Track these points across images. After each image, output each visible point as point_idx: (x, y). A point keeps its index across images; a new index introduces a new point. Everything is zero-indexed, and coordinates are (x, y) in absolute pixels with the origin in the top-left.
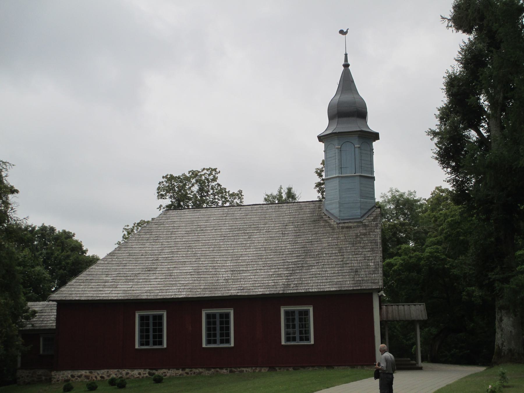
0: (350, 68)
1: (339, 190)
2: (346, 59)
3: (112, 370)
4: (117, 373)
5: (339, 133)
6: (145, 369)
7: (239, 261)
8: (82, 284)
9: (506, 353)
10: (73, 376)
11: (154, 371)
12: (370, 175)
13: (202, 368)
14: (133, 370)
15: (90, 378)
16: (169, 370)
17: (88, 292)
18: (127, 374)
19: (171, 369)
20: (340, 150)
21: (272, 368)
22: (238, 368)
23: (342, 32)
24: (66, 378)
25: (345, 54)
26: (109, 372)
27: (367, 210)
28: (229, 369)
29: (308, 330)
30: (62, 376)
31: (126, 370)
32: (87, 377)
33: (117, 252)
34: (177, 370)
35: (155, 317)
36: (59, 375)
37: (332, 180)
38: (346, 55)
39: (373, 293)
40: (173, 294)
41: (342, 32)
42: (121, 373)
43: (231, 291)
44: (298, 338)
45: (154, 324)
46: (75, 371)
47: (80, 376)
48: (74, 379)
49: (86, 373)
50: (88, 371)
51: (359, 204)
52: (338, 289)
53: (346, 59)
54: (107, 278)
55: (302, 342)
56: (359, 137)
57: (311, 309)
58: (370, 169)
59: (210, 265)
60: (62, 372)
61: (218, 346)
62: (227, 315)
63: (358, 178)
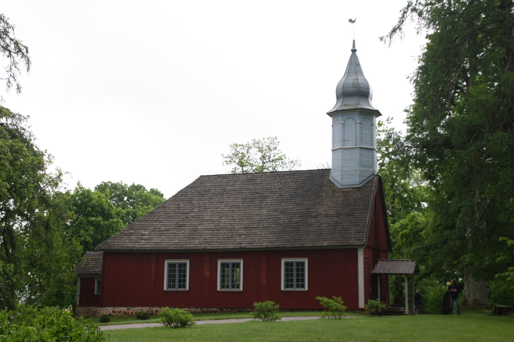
1: (342, 160)
2: (354, 46)
3: (144, 308)
5: (342, 110)
7: (252, 220)
8: (124, 237)
9: (471, 303)
10: (114, 312)
12: (370, 147)
15: (128, 314)
17: (127, 243)
20: (344, 125)
23: (351, 21)
27: (366, 178)
29: (168, 277)
30: (105, 311)
33: (156, 211)
36: (104, 311)
38: (354, 41)
40: (195, 246)
41: (351, 21)
43: (242, 245)
46: (115, 308)
47: (119, 312)
48: (115, 314)
50: (126, 308)
51: (358, 172)
52: (329, 244)
53: (354, 46)
54: (145, 232)
56: (360, 113)
57: (306, 261)
58: (370, 142)
59: (228, 222)
60: (106, 308)
62: (303, 264)
63: (358, 150)
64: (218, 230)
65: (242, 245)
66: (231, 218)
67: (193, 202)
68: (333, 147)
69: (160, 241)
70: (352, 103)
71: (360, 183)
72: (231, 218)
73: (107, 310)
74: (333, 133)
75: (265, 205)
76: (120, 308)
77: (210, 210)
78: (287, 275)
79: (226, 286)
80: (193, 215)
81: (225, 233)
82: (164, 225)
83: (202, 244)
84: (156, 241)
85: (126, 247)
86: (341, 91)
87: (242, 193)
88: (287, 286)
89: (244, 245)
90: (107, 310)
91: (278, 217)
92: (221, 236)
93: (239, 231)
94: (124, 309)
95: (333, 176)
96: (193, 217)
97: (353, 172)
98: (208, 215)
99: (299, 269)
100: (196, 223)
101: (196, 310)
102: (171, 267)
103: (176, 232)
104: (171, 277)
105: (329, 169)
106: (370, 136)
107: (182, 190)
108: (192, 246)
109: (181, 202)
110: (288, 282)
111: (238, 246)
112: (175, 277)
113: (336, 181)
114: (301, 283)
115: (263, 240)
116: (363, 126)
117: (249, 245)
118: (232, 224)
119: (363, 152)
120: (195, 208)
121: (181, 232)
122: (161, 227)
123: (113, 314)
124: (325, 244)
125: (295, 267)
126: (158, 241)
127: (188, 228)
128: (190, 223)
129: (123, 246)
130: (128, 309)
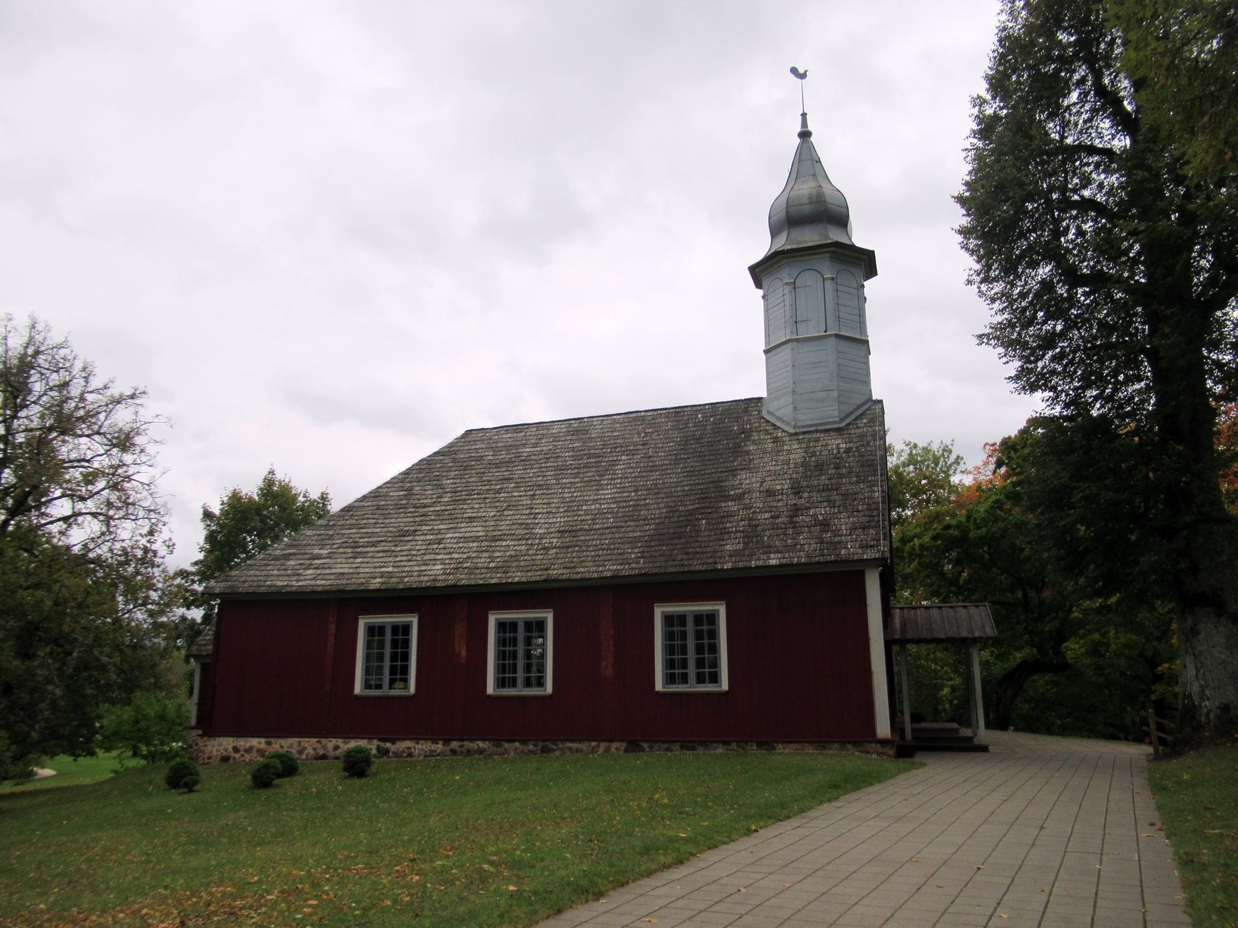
0: (812, 139)
3: (307, 739)
4: (317, 746)
6: (370, 739)
11: (388, 745)
13: (483, 740)
14: (348, 740)
16: (418, 743)
18: (336, 748)
19: (421, 742)
21: (634, 746)
22: (559, 742)
23: (794, 71)
24: (225, 754)
25: (802, 115)
26: (302, 744)
27: (855, 407)
28: (540, 744)
31: (334, 741)
32: (261, 752)
34: (432, 743)
35: (395, 629)
37: (778, 350)
38: (804, 115)
39: (866, 571)
41: (794, 71)
42: (324, 747)
43: (551, 572)
44: (692, 676)
45: (395, 644)
46: (239, 739)
47: (248, 751)
48: (237, 756)
49: (259, 743)
50: (263, 740)
51: (835, 394)
55: (701, 685)
57: (721, 609)
61: (691, 690)
62: (712, 618)
63: (833, 339)
64: (494, 539)
65: (551, 572)
66: (528, 512)
67: (444, 482)
68: (767, 343)
69: (351, 571)
70: (809, 237)
71: (842, 420)
72: (528, 512)
73: (220, 745)
74: (767, 311)
75: (612, 479)
76: (249, 739)
77: (479, 497)
78: (669, 650)
79: (534, 681)
80: (438, 509)
81: (508, 546)
82: (366, 533)
83: (449, 574)
84: (342, 571)
85: (268, 586)
86: (783, 214)
87: (557, 457)
88: (670, 679)
89: (554, 573)
90: (220, 745)
91: (642, 503)
92: (498, 554)
93: (544, 541)
94: (259, 743)
95: (771, 410)
96: (438, 514)
97: (821, 395)
98: (472, 508)
99: (703, 631)
100: (442, 527)
101: (434, 747)
102: (504, 645)
103: (393, 548)
104: (504, 659)
105: (760, 399)
106: (856, 312)
107: (422, 460)
108: (426, 578)
109: (416, 484)
110: (674, 668)
111: (535, 576)
112: (515, 657)
113: (780, 419)
114: (400, 672)
115: (604, 558)
116: (840, 288)
117: (569, 571)
118: (528, 524)
119: (844, 345)
120: (445, 495)
121: (405, 548)
122: (360, 538)
123: (233, 754)
124: (773, 562)
125: (690, 627)
126: (346, 571)
127: (422, 537)
128: (430, 528)
129: (263, 583)
130: (269, 744)
